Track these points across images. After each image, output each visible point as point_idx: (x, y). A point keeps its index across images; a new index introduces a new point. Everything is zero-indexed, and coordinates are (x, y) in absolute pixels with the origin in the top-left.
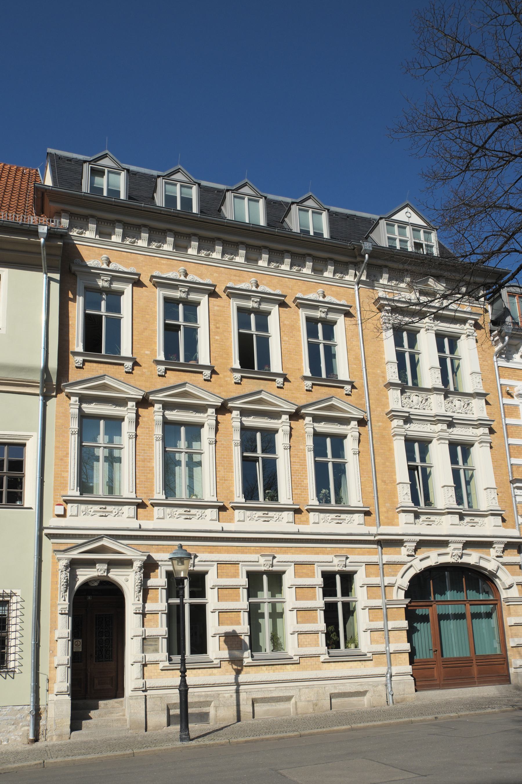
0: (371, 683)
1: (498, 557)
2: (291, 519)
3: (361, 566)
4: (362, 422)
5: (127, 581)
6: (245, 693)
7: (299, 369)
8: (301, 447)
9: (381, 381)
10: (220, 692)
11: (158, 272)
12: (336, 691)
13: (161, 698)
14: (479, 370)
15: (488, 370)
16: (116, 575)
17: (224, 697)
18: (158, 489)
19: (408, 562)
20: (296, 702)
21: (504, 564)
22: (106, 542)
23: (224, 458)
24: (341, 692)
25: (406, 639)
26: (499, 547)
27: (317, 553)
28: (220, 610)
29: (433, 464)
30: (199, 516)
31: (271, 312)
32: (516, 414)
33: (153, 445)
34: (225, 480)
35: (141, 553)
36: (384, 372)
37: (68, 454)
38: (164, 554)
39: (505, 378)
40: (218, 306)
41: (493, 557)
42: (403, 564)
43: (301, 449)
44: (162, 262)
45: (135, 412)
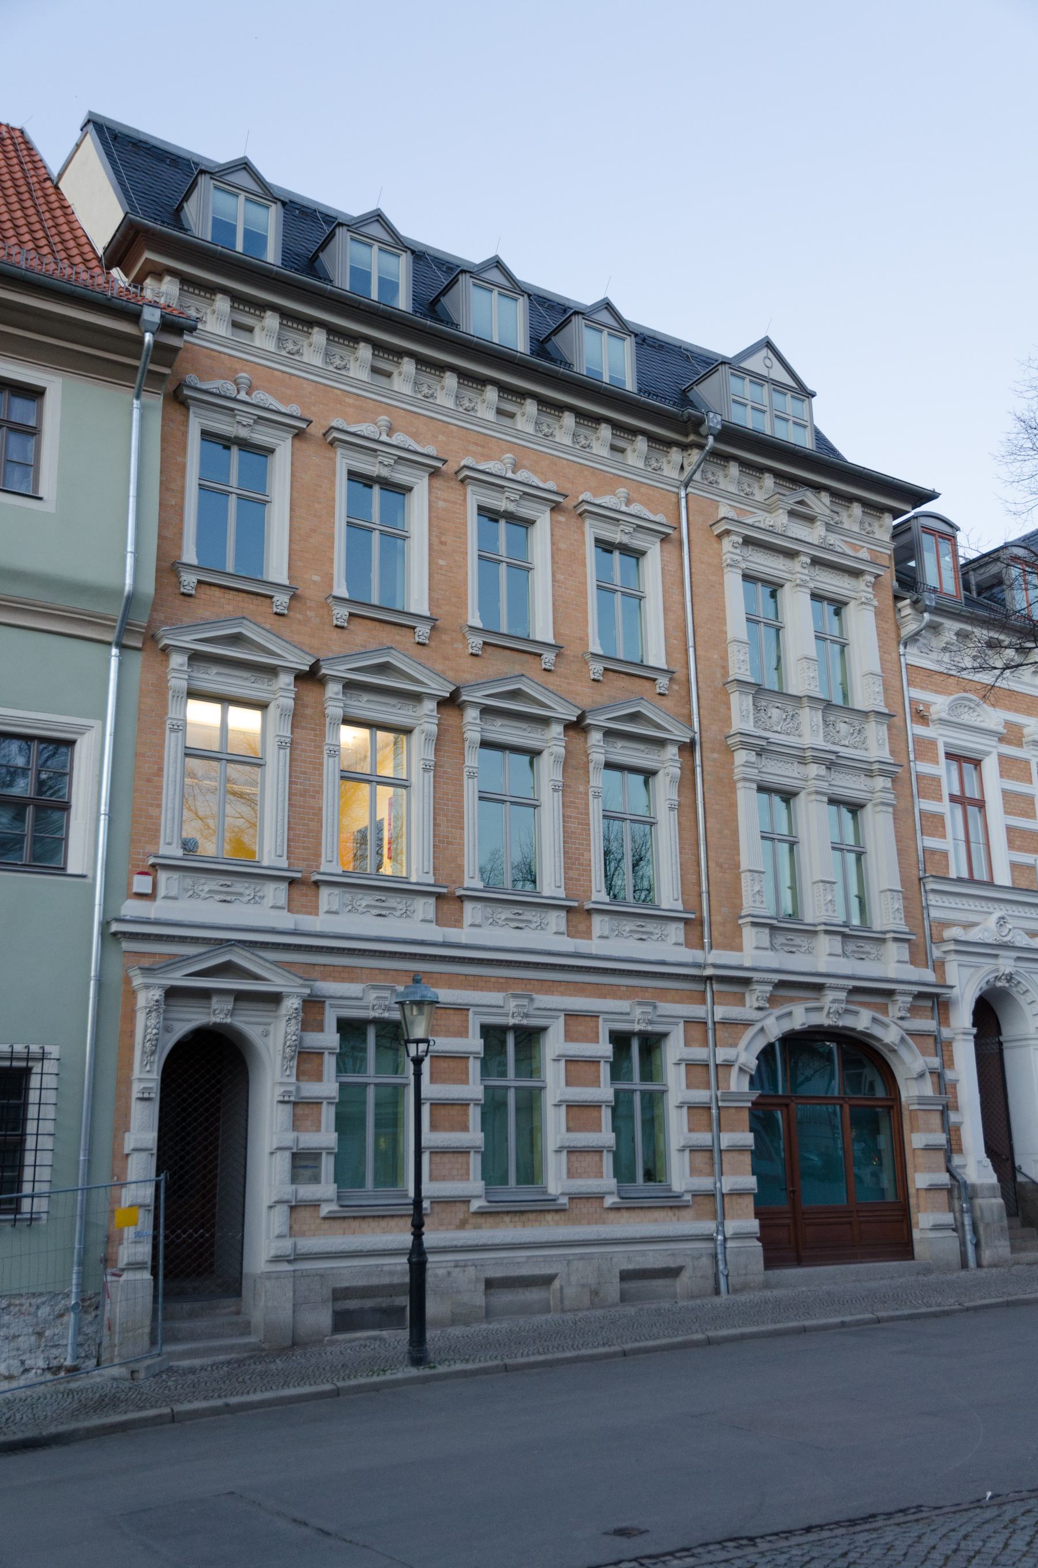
0: (690, 1252)
1: (902, 1018)
2: (282, 900)
3: (677, 1024)
4: (688, 748)
5: (266, 1036)
6: (474, 1268)
7: (581, 639)
8: (582, 789)
9: (719, 675)
11: (341, 421)
12: (631, 1267)
13: (322, 1276)
14: (878, 669)
15: (891, 670)
16: (246, 1023)
17: (436, 1276)
18: (329, 854)
19: (757, 1021)
20: (561, 1288)
21: (912, 1034)
22: (241, 958)
23: (448, 800)
24: (638, 1267)
25: (750, 1168)
26: (903, 1001)
27: (603, 996)
29: (800, 837)
30: (250, 898)
31: (535, 521)
32: (930, 755)
33: (322, 764)
34: (449, 843)
35: (301, 982)
36: (724, 658)
37: (161, 769)
38: (336, 984)
39: (915, 687)
40: (445, 500)
41: (892, 1019)
42: (747, 1024)
43: (581, 793)
44: (347, 400)
45: (293, 696)
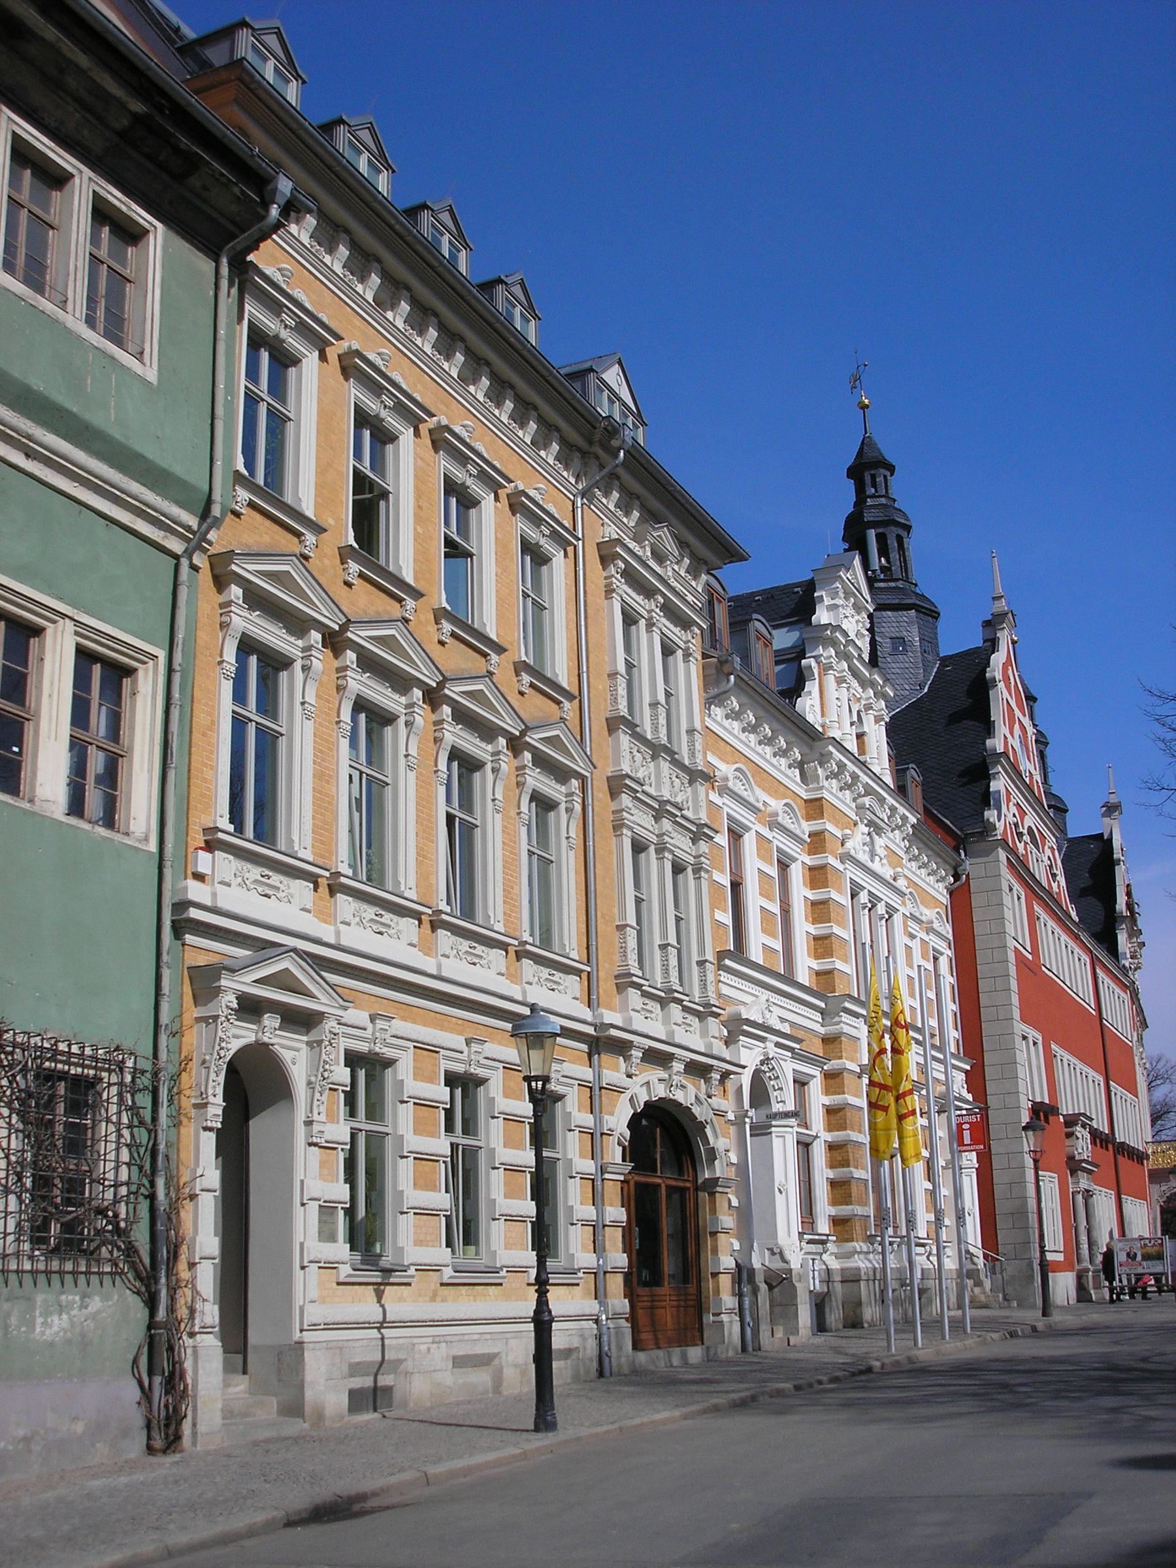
10: (415, 1341)
13: (341, 1348)
28: (418, 1153)
44: (355, 321)
